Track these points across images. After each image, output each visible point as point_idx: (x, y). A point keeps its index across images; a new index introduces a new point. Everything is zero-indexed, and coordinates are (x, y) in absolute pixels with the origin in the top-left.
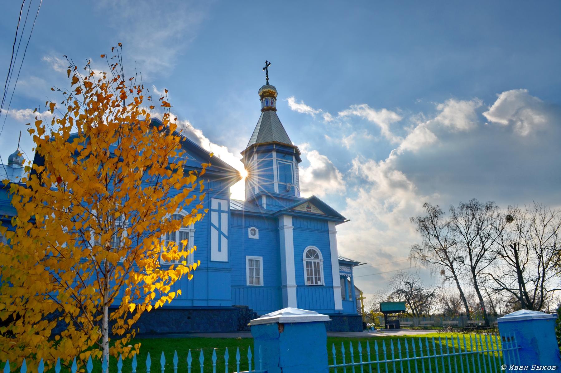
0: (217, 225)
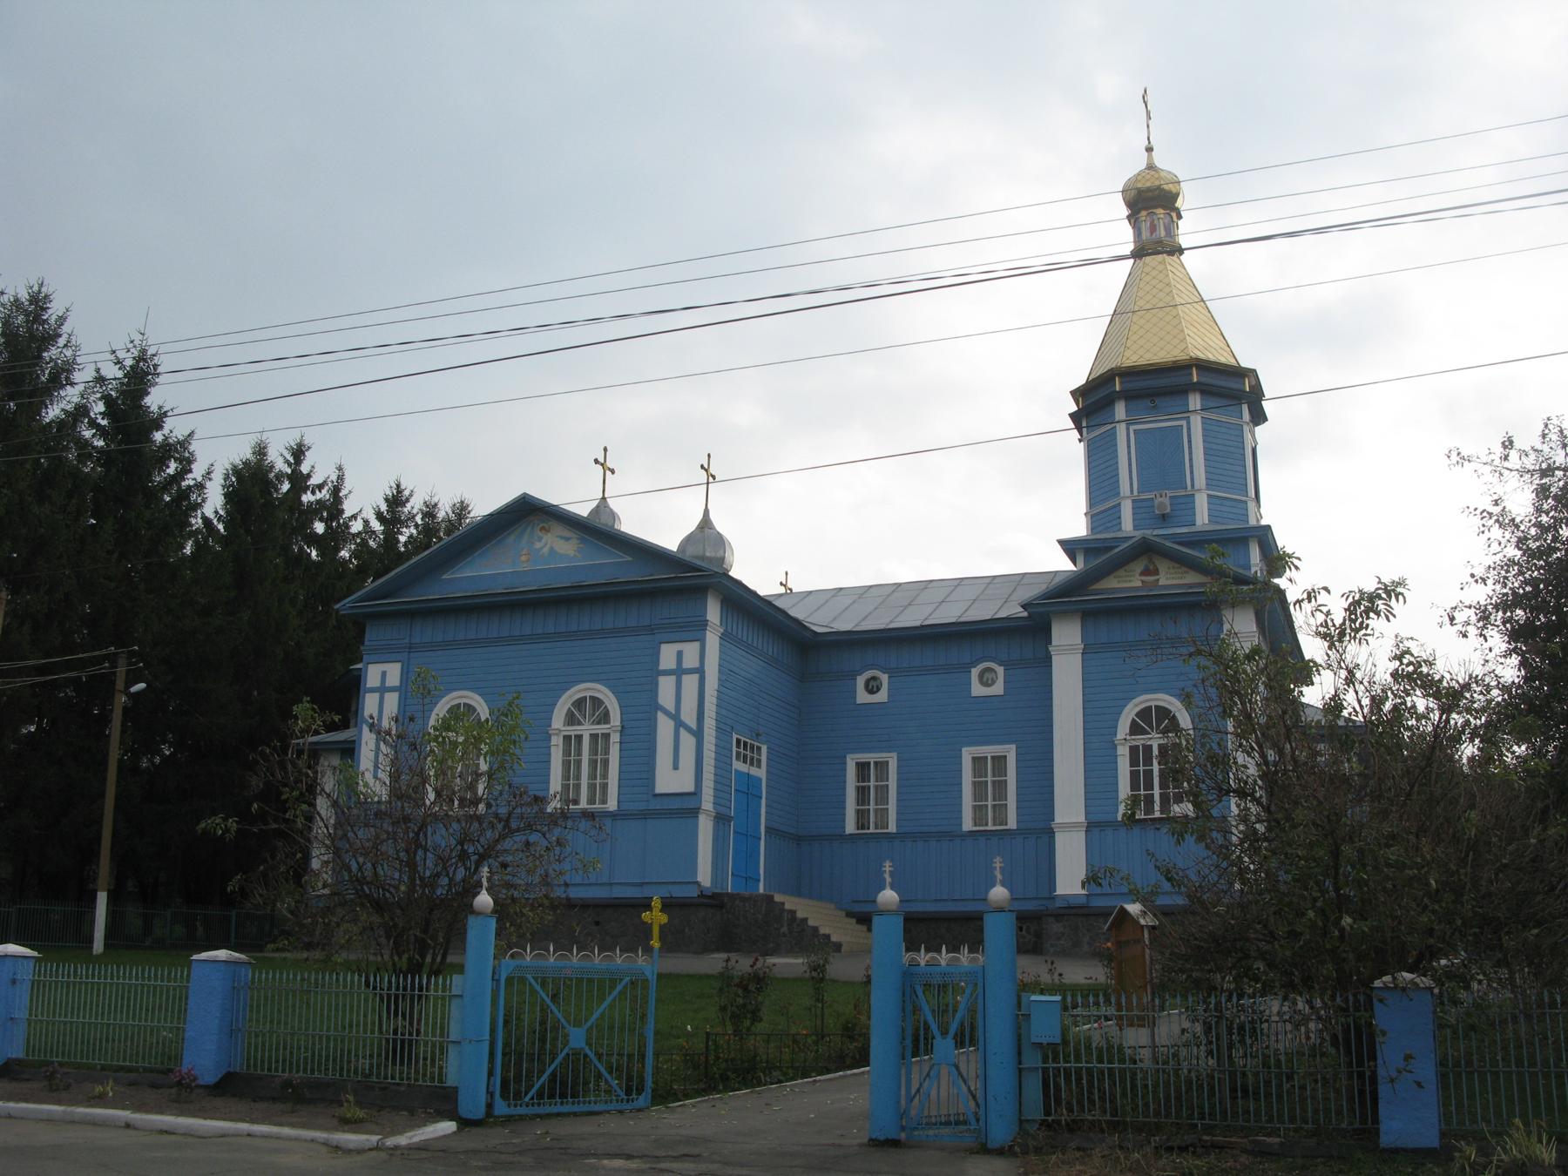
0: (671, 708)
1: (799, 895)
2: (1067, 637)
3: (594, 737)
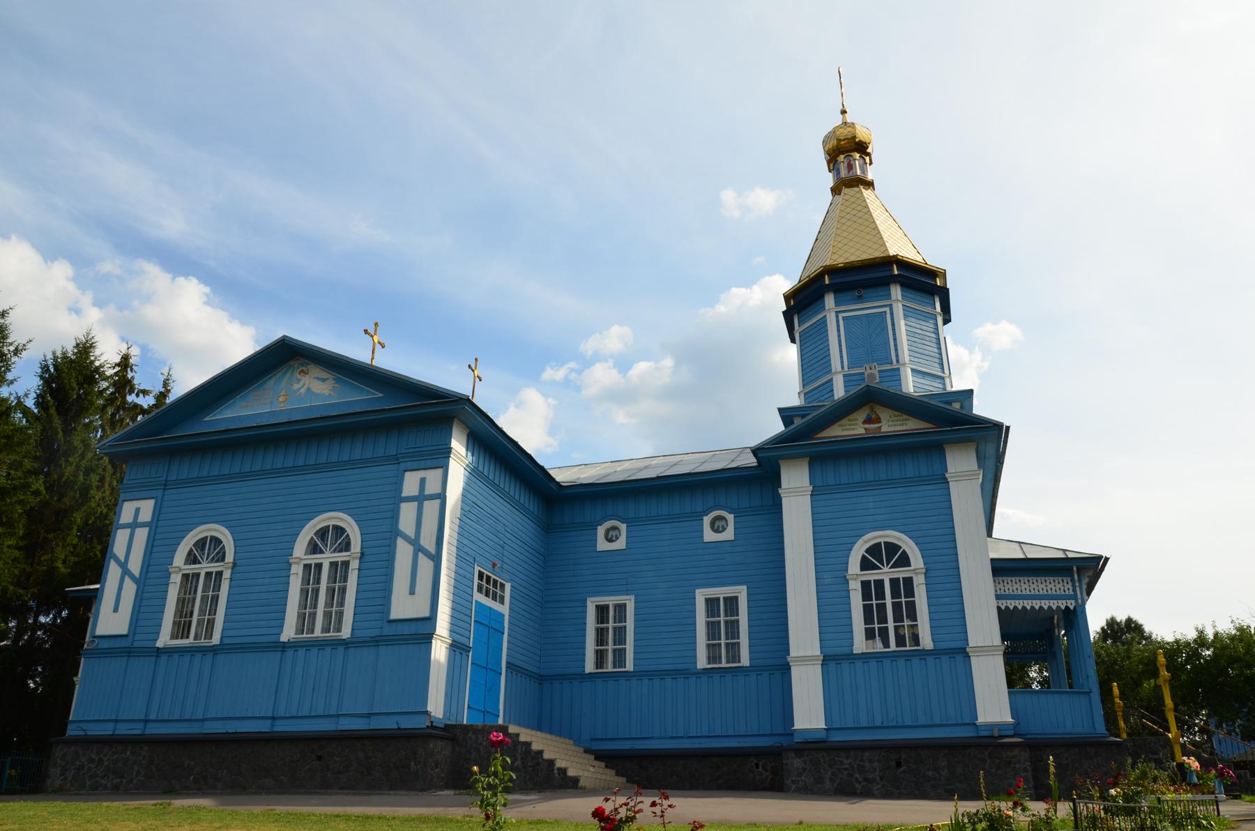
0: (410, 532)
1: (539, 728)
2: (795, 482)
3: (334, 565)
